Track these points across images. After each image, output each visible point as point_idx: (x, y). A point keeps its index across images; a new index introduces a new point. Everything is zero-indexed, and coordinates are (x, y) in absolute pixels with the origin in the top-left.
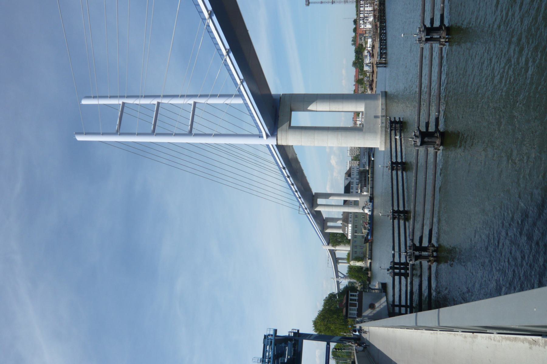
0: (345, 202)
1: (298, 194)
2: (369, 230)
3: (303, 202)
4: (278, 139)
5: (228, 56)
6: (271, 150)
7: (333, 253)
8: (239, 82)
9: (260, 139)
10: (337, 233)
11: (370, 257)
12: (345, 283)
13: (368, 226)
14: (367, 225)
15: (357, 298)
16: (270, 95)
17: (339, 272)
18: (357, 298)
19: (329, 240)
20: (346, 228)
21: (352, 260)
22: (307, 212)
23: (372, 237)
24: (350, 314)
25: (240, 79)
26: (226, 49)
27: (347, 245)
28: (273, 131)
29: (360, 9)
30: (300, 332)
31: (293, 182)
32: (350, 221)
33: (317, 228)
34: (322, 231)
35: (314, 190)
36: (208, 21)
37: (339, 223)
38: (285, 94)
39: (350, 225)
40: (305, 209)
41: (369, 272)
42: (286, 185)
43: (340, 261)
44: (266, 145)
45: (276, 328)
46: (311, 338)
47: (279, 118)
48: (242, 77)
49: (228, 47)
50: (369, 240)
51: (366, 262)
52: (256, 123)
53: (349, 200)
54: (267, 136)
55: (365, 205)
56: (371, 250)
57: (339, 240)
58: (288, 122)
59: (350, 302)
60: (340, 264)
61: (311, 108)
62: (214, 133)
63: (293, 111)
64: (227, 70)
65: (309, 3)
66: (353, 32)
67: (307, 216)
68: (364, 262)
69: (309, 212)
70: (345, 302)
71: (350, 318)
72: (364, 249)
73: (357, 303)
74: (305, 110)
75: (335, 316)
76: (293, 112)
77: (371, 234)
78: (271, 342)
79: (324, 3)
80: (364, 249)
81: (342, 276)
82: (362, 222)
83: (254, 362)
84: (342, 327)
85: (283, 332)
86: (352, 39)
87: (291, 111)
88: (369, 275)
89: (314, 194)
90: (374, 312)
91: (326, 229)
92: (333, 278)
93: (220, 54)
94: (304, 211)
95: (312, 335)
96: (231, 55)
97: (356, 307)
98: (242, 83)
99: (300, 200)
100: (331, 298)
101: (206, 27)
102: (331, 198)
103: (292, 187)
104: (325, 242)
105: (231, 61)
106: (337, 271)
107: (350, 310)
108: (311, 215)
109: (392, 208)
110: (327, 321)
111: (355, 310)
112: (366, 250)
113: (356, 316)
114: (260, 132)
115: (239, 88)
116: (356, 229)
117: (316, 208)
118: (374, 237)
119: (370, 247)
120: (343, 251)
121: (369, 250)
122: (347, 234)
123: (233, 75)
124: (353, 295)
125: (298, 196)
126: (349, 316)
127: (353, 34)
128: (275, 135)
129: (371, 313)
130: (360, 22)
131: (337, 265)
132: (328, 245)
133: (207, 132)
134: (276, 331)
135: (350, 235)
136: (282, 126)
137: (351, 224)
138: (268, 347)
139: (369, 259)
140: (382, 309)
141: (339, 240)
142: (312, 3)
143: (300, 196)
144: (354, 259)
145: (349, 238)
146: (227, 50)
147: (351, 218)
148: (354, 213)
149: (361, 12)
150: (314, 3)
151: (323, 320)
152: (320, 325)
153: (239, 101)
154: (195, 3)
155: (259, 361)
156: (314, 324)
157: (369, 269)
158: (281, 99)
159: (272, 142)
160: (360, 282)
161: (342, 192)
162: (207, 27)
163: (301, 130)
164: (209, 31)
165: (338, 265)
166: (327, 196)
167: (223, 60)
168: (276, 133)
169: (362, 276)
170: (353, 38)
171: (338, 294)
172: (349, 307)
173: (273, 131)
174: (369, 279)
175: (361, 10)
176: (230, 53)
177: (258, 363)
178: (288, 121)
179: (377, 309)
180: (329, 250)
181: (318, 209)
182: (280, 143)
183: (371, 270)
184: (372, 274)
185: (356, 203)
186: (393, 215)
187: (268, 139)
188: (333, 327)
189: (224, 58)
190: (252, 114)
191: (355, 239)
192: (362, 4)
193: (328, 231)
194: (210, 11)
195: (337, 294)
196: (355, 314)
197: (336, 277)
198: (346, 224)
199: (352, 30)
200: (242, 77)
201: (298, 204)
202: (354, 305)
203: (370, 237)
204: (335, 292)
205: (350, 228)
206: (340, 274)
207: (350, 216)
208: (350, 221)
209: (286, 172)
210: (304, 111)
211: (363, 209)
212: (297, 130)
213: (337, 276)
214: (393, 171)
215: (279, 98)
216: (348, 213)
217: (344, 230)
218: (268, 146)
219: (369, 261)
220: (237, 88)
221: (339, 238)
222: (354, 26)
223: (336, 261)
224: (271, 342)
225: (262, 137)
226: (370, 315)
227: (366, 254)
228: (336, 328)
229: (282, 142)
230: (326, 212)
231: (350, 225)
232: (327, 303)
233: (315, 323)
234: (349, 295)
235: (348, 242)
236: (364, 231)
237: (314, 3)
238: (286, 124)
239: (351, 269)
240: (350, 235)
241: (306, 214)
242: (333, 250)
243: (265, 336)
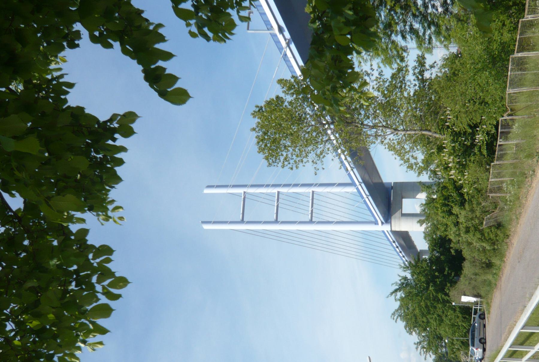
3: (404, 255)
5: (288, 48)
8: (365, 196)
16: (382, 184)
25: (285, 39)
28: (388, 216)
31: (394, 240)
40: (392, 243)
47: (392, 206)
54: (382, 223)
58: (401, 210)
62: (336, 220)
63: (405, 198)
64: (278, 49)
69: (398, 245)
70: (431, 295)
74: (414, 197)
76: (404, 200)
87: (402, 198)
89: (419, 251)
93: (261, 11)
94: (401, 258)
96: (293, 46)
98: (288, 45)
114: (377, 221)
133: (331, 220)
136: (395, 213)
153: (352, 189)
159: (387, 228)
163: (412, 217)
168: (389, 221)
173: (388, 216)
176: (291, 44)
178: (400, 209)
182: (393, 229)
190: (292, 67)
212: (409, 217)
218: (383, 232)
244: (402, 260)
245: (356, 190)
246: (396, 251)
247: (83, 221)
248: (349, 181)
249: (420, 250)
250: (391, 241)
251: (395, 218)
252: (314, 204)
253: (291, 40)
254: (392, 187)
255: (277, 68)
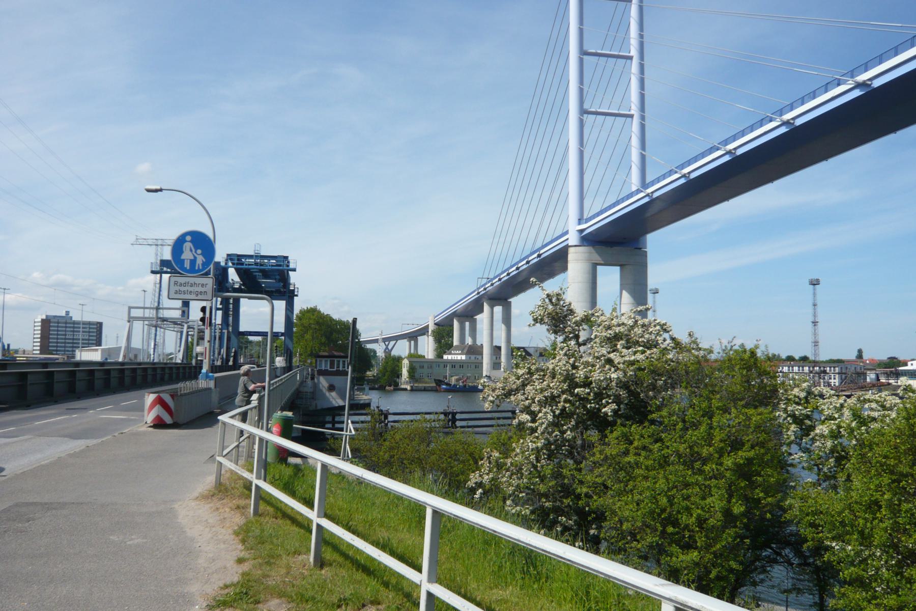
0: (499, 348)
1: (513, 271)
2: (455, 386)
3: (495, 285)
4: (577, 248)
5: (724, 152)
6: (610, 209)
7: (423, 331)
8: (686, 171)
9: (577, 221)
10: (452, 337)
11: (414, 388)
12: (379, 350)
13: (461, 384)
14: (463, 382)
15: (341, 368)
17: (395, 342)
18: (341, 368)
19: (442, 326)
20: (460, 352)
21: (410, 362)
22: (480, 290)
23: (444, 391)
24: (321, 361)
26: (735, 149)
27: (436, 353)
28: (588, 240)
29: (806, 366)
30: (295, 297)
32: (470, 358)
33: (459, 307)
34: (455, 315)
35: (514, 301)
36: (850, 82)
37: (469, 341)
38: (646, 256)
39: (464, 357)
41: (392, 388)
42: (516, 259)
43: (413, 342)
44: (568, 231)
45: (297, 270)
46: (288, 312)
48: (693, 176)
49: (740, 152)
50: (440, 386)
51: (407, 383)
52: (623, 200)
53: (500, 355)
54: (581, 231)
55: (493, 379)
56: (425, 390)
57: (443, 341)
58: (603, 262)
59: (336, 360)
60: (407, 343)
61: (625, 294)
65: (814, 285)
66: (787, 355)
67: (474, 291)
68: (407, 379)
71: (316, 361)
72: (427, 379)
73: (335, 370)
74: (622, 287)
75: (323, 340)
76: (618, 268)
77: (448, 389)
78: (280, 266)
79: (815, 309)
80: (427, 379)
81: (390, 347)
82: (469, 375)
83: (255, 246)
84: (309, 349)
85: (293, 277)
86: (777, 354)
87: (621, 266)
88: (387, 388)
90: (324, 390)
91: (458, 321)
92: (381, 334)
93: (794, 104)
95: (292, 313)
96: (727, 158)
97: (330, 368)
98: (684, 176)
99: (514, 268)
100: (350, 329)
101: (836, 78)
102: (503, 327)
103: (535, 255)
104: (438, 319)
105: (770, 130)
106: (397, 338)
107: (326, 361)
108: (476, 296)
109: (458, 411)
110: (315, 329)
111: (325, 367)
112: (426, 383)
113: (318, 368)
114: (587, 221)
115: (676, 172)
116: (457, 366)
117: (487, 303)
118: (444, 393)
119: (430, 389)
120: (427, 347)
121: (425, 387)
122: (450, 354)
123: (743, 136)
124: (344, 364)
125: (510, 271)
126: (318, 359)
127: (784, 357)
128: (583, 243)
129: (323, 386)
130: (786, 366)
131: (406, 338)
132: (435, 324)
134: (294, 270)
135: (450, 357)
136: (597, 252)
137: (466, 359)
138: (275, 261)
139: (412, 387)
140: (328, 399)
141: (443, 341)
142: (814, 289)
143: (511, 275)
144: (412, 365)
145: (445, 357)
146: (792, 122)
147: (475, 358)
148: (482, 363)
149: (832, 368)
150: (815, 294)
151: (318, 323)
152: (310, 319)
154: (829, 85)
155: (256, 252)
156: (311, 308)
157: (397, 388)
158: (638, 250)
159: (573, 238)
160: (377, 374)
161: (515, 343)
162: (768, 119)
163: (591, 281)
164: (764, 121)
165: (406, 340)
166: (507, 320)
167: (719, 144)
168: (585, 244)
169: (386, 377)
170: (779, 355)
171: (359, 341)
172: (329, 359)
173: (588, 240)
174: (382, 388)
175: (794, 368)
176: (786, 128)
177: (255, 250)
178: (603, 261)
179: (327, 394)
180: (428, 326)
181: (486, 307)
182: (571, 250)
183: (395, 390)
184: (389, 391)
185: (496, 365)
186: (449, 413)
187: (576, 232)
188: (308, 336)
189: (722, 145)
191: (442, 365)
192: (834, 370)
193: (456, 324)
194: (872, 84)
195: (359, 340)
196: (321, 367)
197: (383, 339)
198: (465, 351)
199: (790, 355)
200: (693, 175)
201: (491, 276)
202: (332, 366)
203: (443, 388)
204: (362, 337)
205: (459, 357)
206: (392, 343)
207: (478, 357)
208: (470, 358)
209: (534, 259)
210: (621, 285)
211: (486, 376)
213: (384, 340)
214: (510, 413)
215: (641, 247)
216: (482, 354)
217: (457, 348)
218: (567, 233)
219: (409, 388)
220: (676, 168)
221: (445, 341)
222: (797, 358)
223: (413, 337)
224: (280, 266)
225: (579, 224)
226: (321, 385)
227: (420, 382)
228: (306, 340)
229: (572, 254)
230: (482, 319)
231: (464, 357)
232: (345, 326)
233: (313, 311)
234: (344, 359)
235: (440, 356)
236: (453, 379)
237: (815, 294)
238: (600, 259)
239: (399, 360)
240: (450, 357)
241: (478, 289)
242: (428, 332)
243: (286, 258)
244: (495, 278)
245: (634, 188)
246: (512, 267)
247: (199, 265)
248: (649, 179)
249: (510, 302)
250: (542, 252)
251: (590, 253)
252: (614, 118)
253: (735, 156)
254: (641, 249)
255: (900, 25)
